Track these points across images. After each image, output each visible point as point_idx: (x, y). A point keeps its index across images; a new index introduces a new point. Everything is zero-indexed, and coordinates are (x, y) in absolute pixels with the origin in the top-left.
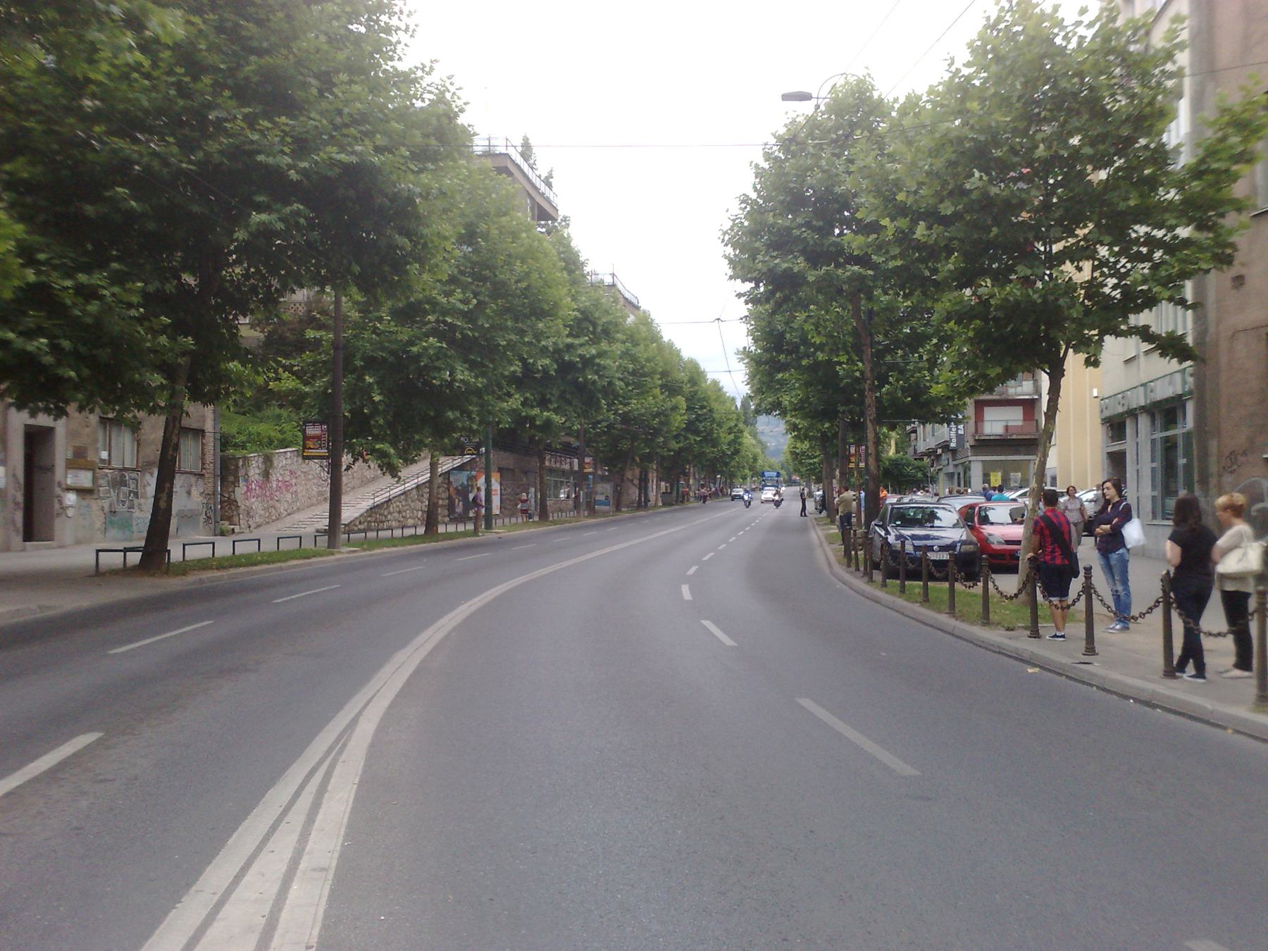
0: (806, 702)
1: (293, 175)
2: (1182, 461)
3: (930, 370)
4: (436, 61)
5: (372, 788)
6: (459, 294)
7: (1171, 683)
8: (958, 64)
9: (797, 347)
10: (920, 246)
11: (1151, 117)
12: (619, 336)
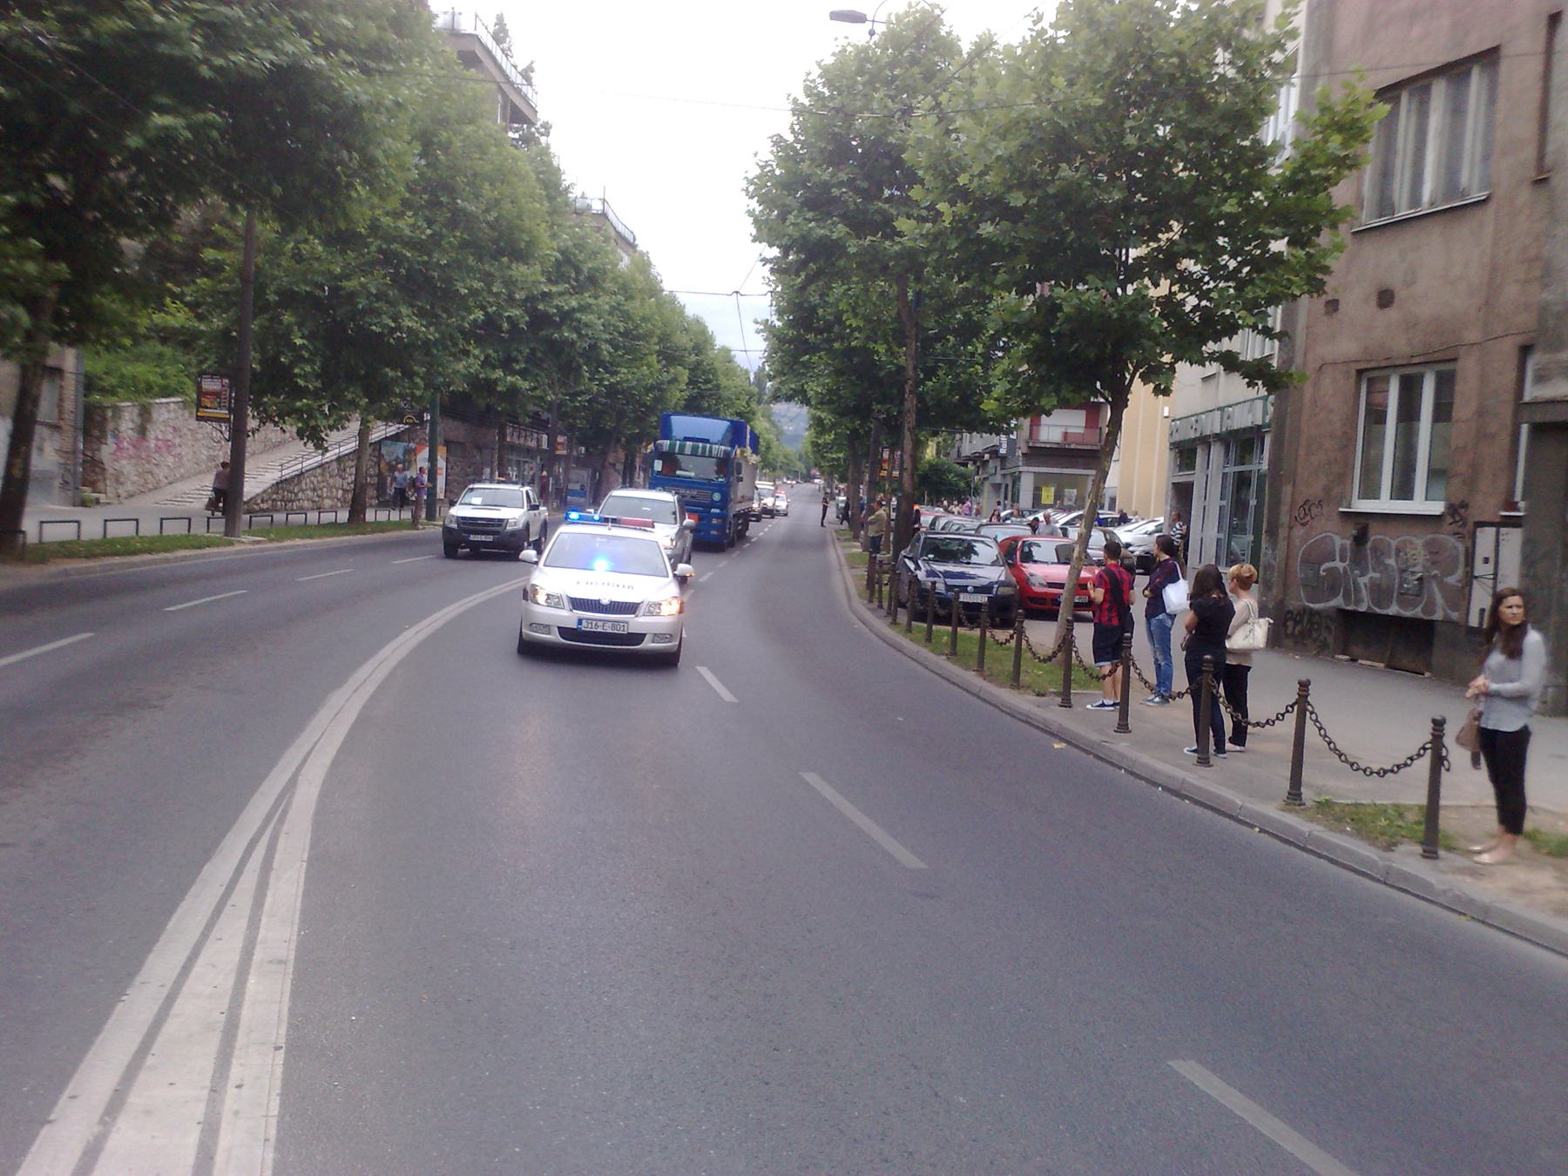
0: (812, 778)
1: (205, 71)
2: (1253, 502)
7: (1203, 770)
8: (1045, 24)
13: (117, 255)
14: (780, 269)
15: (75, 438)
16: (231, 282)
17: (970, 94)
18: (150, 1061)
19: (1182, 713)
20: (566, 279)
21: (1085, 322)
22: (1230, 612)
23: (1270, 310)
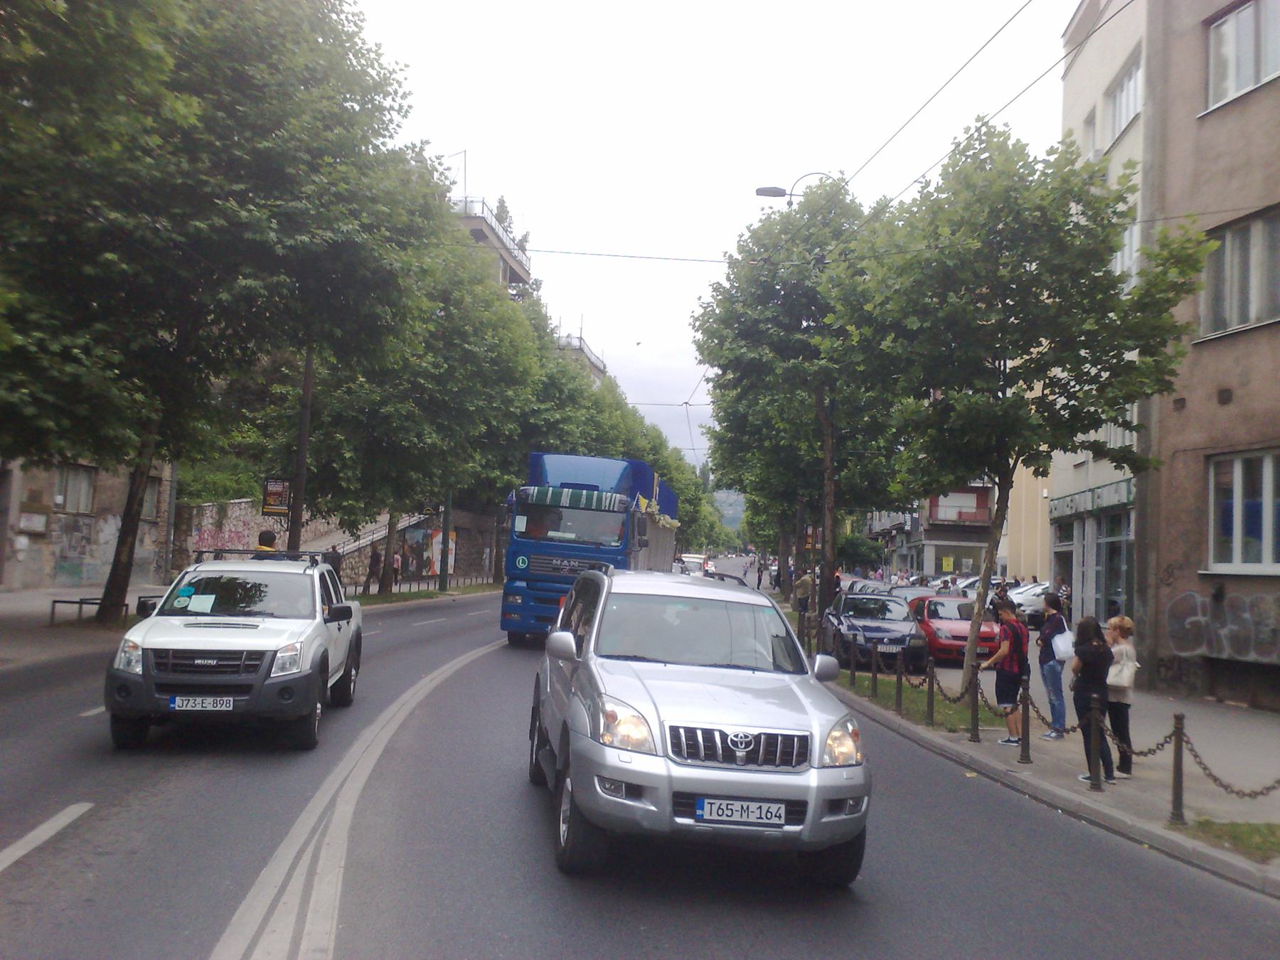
1: (279, 250)
2: (1124, 567)
3: (888, 458)
4: (427, 142)
6: (430, 357)
7: (1096, 795)
10: (883, 355)
11: (1103, 248)
14: (719, 384)
19: (1074, 745)
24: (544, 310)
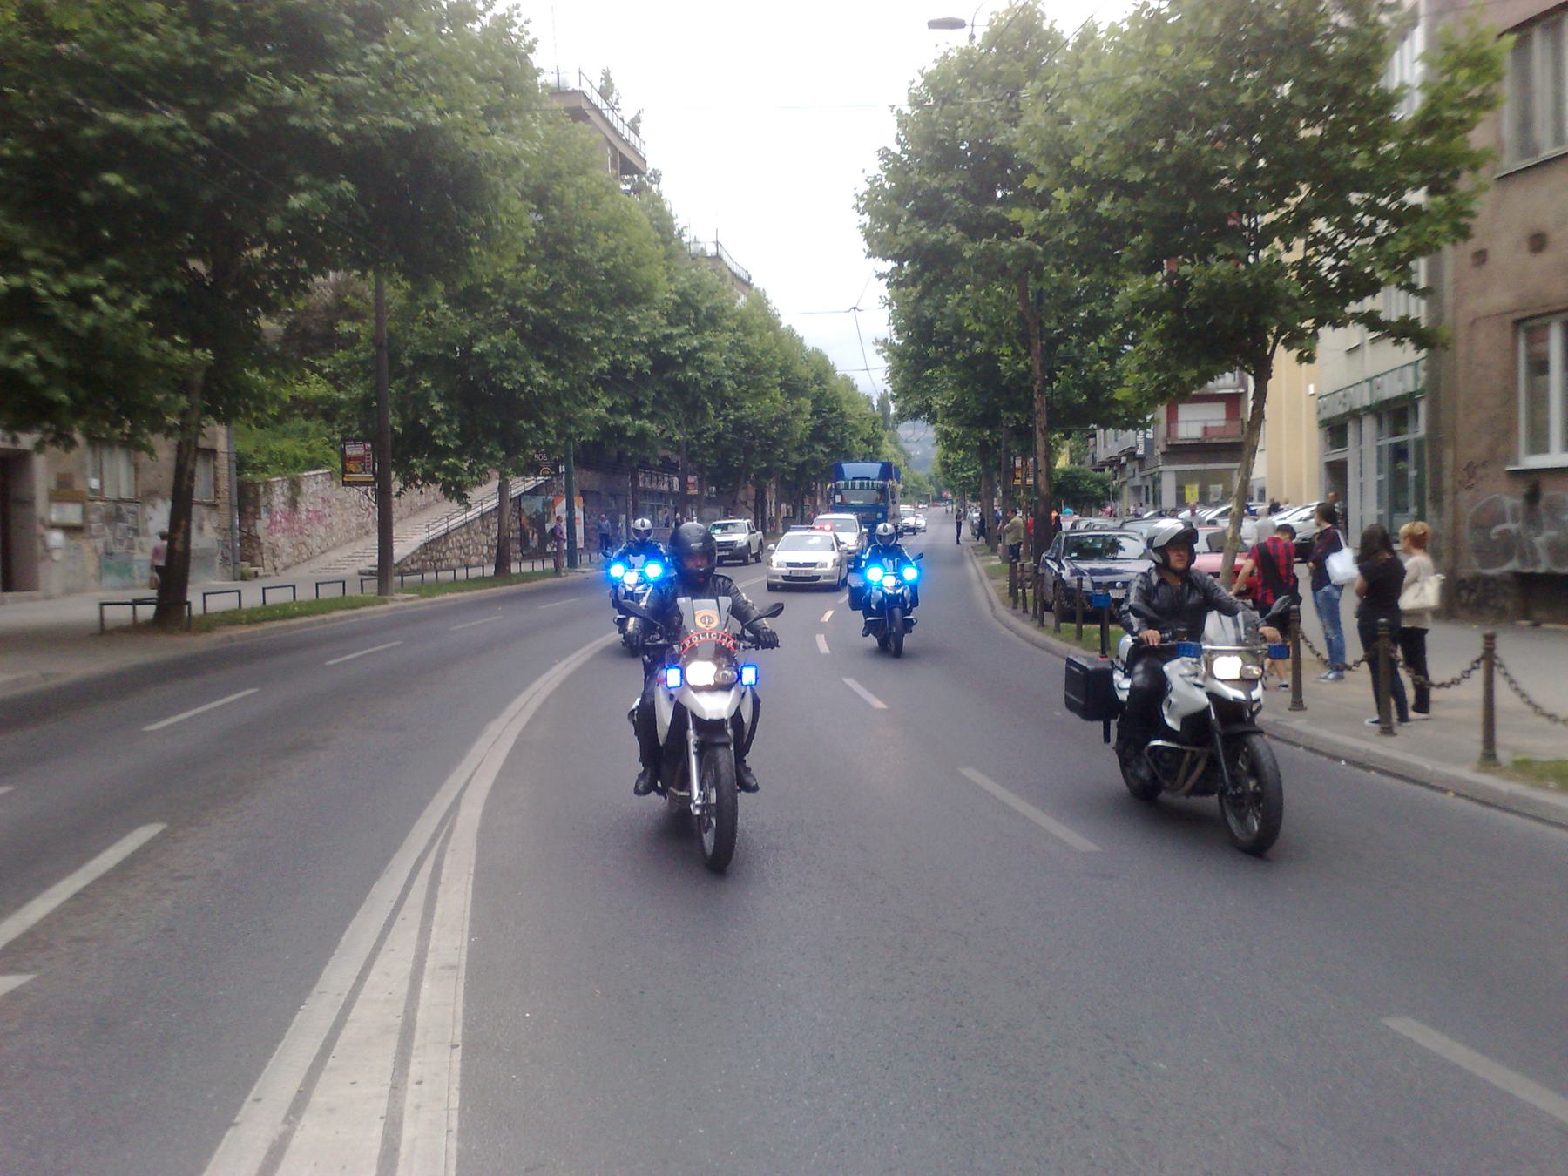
0: (969, 772)
1: (335, 139)
2: (1412, 473)
3: (1112, 362)
5: (488, 880)
7: (1389, 740)
9: (948, 340)
10: (1100, 221)
12: (727, 323)
13: (257, 333)
14: (896, 282)
15: (232, 517)
16: (367, 350)
17: (1076, 74)
18: (331, 1062)
19: (1359, 685)
20: (686, 321)
21: (1218, 296)
22: (1403, 572)
23: (1412, 264)
24: (667, 207)
